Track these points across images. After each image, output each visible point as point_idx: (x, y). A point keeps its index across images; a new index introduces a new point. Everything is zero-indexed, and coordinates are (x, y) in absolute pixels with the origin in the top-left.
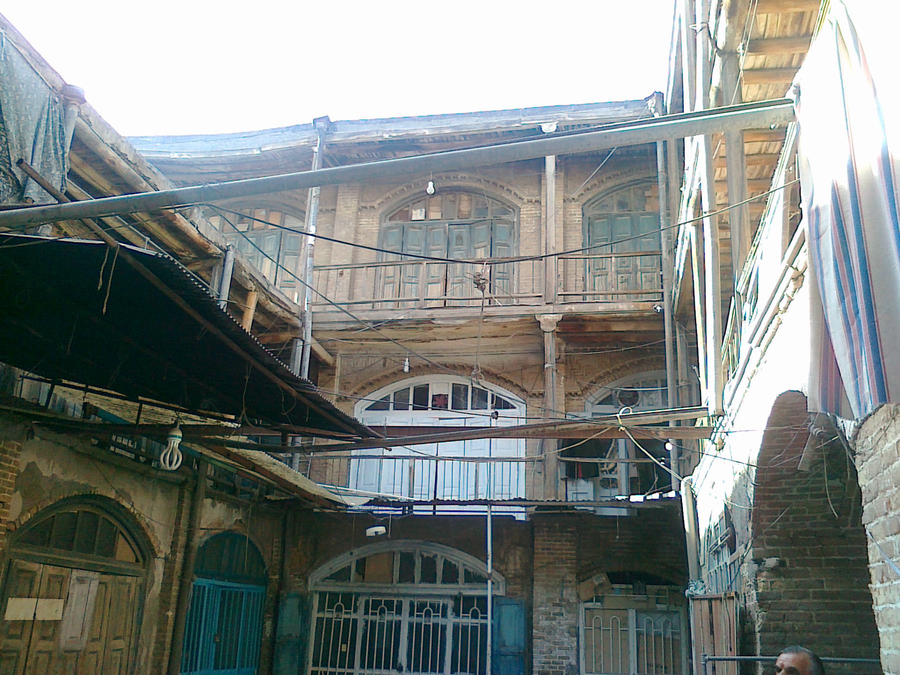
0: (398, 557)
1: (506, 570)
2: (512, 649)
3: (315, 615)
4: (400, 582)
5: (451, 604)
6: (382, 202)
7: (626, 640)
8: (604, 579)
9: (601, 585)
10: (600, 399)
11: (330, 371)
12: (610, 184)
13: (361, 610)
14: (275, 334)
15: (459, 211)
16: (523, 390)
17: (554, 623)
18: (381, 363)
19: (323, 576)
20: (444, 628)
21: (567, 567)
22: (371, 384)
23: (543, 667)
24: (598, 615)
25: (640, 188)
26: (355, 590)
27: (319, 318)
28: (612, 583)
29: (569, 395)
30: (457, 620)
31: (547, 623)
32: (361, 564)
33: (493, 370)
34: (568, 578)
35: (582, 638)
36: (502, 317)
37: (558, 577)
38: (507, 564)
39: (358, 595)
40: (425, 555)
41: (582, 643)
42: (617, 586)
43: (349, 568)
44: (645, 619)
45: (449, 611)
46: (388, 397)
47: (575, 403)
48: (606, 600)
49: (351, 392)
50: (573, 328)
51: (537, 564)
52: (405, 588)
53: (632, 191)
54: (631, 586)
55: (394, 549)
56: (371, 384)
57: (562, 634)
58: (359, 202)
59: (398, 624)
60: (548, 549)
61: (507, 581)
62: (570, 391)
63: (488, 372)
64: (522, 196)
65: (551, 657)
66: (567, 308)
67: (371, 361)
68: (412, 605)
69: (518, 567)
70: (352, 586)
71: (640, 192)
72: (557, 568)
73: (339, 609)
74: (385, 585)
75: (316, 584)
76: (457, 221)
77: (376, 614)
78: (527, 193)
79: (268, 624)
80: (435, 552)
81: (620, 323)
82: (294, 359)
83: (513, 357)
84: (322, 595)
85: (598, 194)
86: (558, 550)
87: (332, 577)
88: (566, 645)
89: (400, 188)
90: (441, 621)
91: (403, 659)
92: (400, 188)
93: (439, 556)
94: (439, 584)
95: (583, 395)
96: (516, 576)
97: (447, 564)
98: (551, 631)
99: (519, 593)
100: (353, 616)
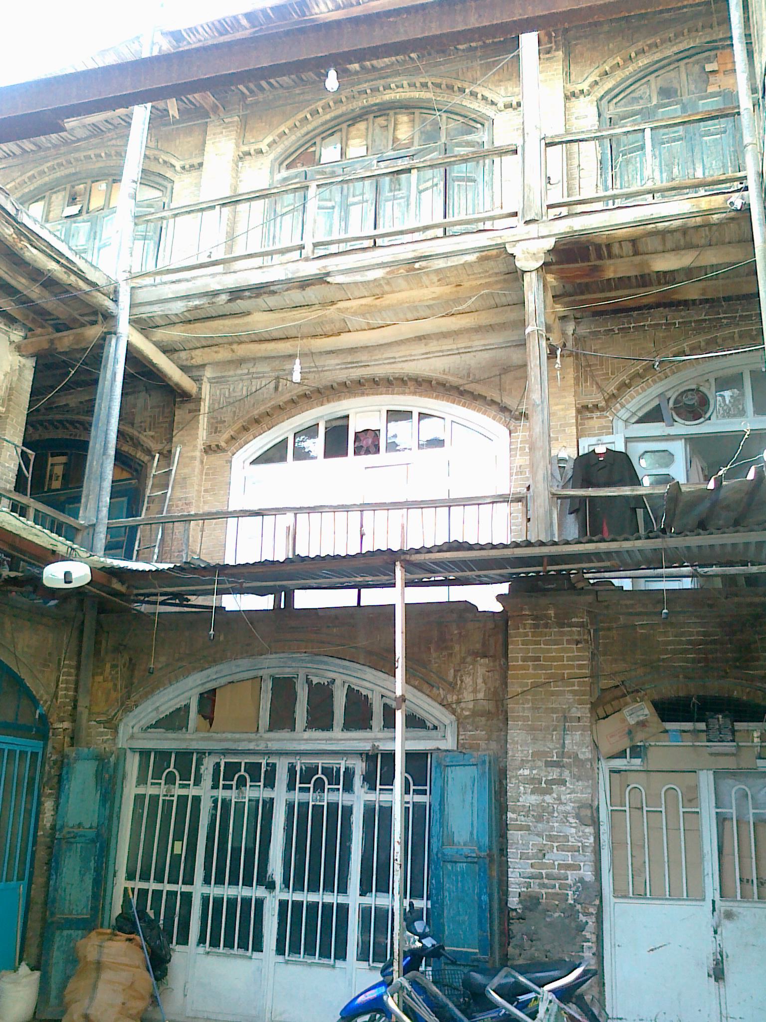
0: (268, 685)
1: (458, 702)
2: (466, 850)
3: (131, 789)
4: (271, 730)
5: (360, 767)
6: (274, 142)
7: (694, 831)
8: (646, 711)
9: (642, 724)
10: (640, 414)
11: (191, 406)
12: (643, 61)
13: (207, 781)
14: (79, 331)
15: (395, 139)
16: (504, 409)
17: (548, 799)
18: (272, 385)
19: (144, 722)
20: (348, 811)
21: (574, 693)
22: (257, 421)
23: (529, 885)
24: (636, 782)
25: (697, 62)
26: (194, 745)
27: (143, 296)
28: (663, 721)
29: (583, 410)
30: (371, 797)
31: (533, 799)
32: (208, 700)
33: (453, 380)
34: (575, 712)
35: (604, 828)
36: (447, 255)
37: (554, 710)
38: (460, 692)
39: (202, 754)
40: (315, 680)
41: (605, 838)
42: (670, 726)
43: (187, 707)
44: (733, 788)
45: (358, 781)
46: (285, 441)
47: (595, 422)
48: (652, 753)
49: (226, 436)
50: (575, 259)
51: (514, 688)
52: (281, 740)
53: (683, 69)
54: (702, 726)
55: (261, 673)
56: (257, 421)
57: (565, 820)
58: (238, 146)
59: (269, 804)
60: (538, 659)
61: (461, 723)
62: (585, 402)
63: (444, 385)
64: (496, 99)
65: (543, 866)
66: (563, 227)
67: (256, 384)
68: (292, 770)
69: (481, 695)
70: (191, 738)
71: (697, 68)
72: (553, 694)
73: (170, 780)
74: (244, 736)
75: (132, 737)
76: (391, 154)
77: (229, 787)
78: (501, 94)
79: (49, 805)
80: (332, 675)
81: (667, 255)
82: (106, 366)
83: (487, 355)
84: (144, 754)
85: (624, 80)
86: (554, 659)
87: (157, 725)
88: (572, 842)
89: (301, 116)
90: (341, 798)
91: (276, 868)
92: (301, 116)
93: (338, 682)
94: (337, 732)
95: (607, 408)
96: (475, 714)
97: (352, 694)
98: (542, 814)
99: (483, 744)
100: (193, 791)
